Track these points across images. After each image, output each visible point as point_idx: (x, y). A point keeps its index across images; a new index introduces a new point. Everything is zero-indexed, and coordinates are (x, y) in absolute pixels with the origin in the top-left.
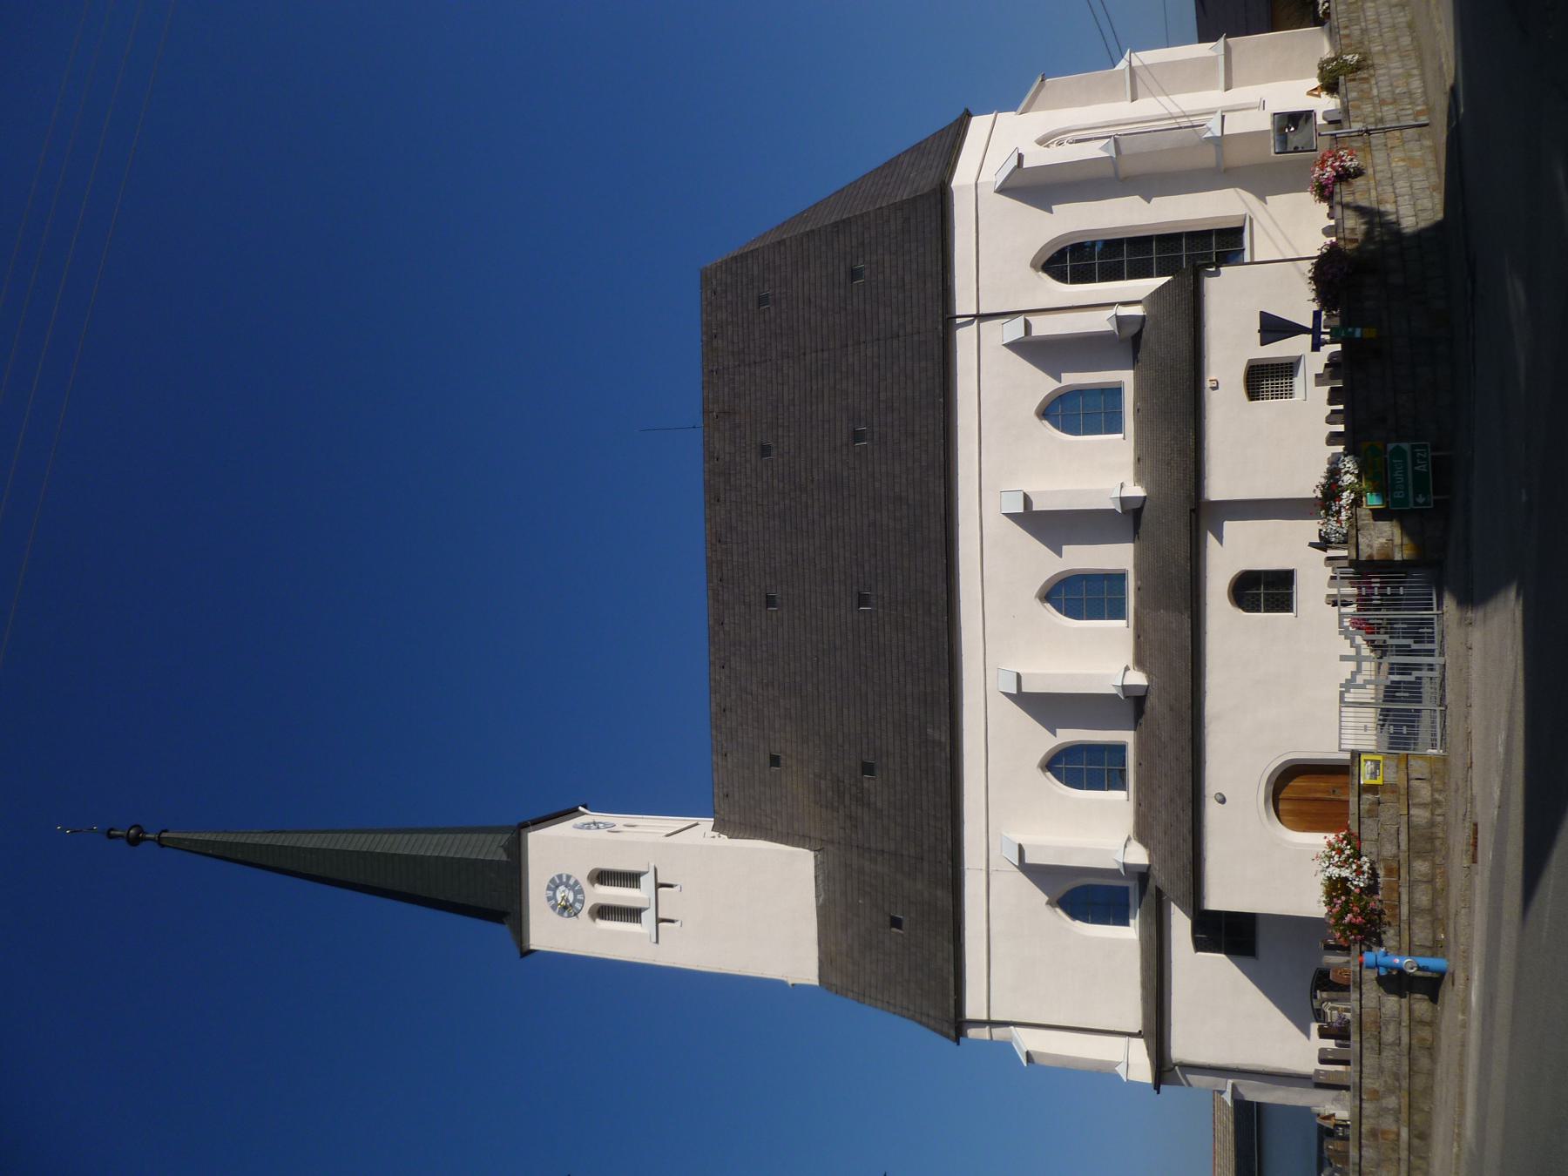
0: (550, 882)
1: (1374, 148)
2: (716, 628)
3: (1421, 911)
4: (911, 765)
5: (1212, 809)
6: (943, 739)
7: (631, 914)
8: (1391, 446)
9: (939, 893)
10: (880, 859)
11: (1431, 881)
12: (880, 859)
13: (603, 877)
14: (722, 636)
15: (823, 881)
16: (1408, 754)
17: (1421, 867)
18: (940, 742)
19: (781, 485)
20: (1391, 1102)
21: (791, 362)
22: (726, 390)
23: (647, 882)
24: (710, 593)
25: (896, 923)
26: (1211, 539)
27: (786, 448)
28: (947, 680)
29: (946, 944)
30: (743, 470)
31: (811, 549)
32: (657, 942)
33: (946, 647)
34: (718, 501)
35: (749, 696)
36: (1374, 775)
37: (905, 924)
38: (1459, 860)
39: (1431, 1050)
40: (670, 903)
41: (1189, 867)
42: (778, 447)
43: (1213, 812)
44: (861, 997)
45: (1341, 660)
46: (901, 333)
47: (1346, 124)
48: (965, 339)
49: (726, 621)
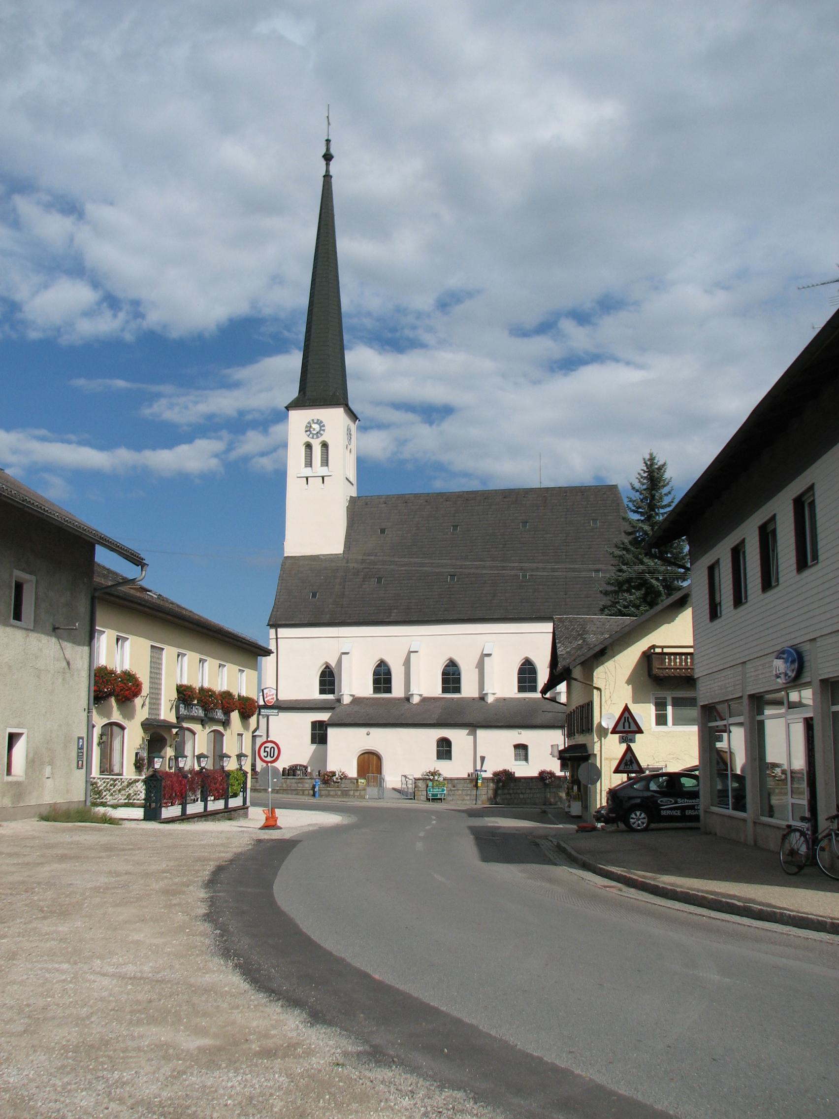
2: (444, 497)
3: (329, 792)
4: (381, 602)
5: (364, 731)
6: (392, 617)
7: (309, 463)
8: (445, 788)
9: (328, 616)
10: (341, 587)
11: (336, 795)
12: (341, 587)
13: (325, 445)
14: (441, 500)
15: (330, 558)
17: (339, 793)
18: (390, 616)
19: (507, 534)
20: (284, 785)
21: (564, 538)
22: (556, 501)
23: (323, 471)
24: (461, 493)
25: (314, 595)
26: (467, 731)
27: (524, 536)
28: (416, 619)
29: (308, 619)
30: (517, 512)
31: (477, 550)
32: (298, 477)
33: (430, 619)
34: (504, 498)
35: (412, 516)
36: (361, 782)
37: (314, 599)
38: (340, 800)
39: (297, 794)
40: (315, 482)
41: (343, 722)
42: (525, 531)
43: (363, 731)
44: (281, 578)
46: (567, 596)
49: (448, 502)
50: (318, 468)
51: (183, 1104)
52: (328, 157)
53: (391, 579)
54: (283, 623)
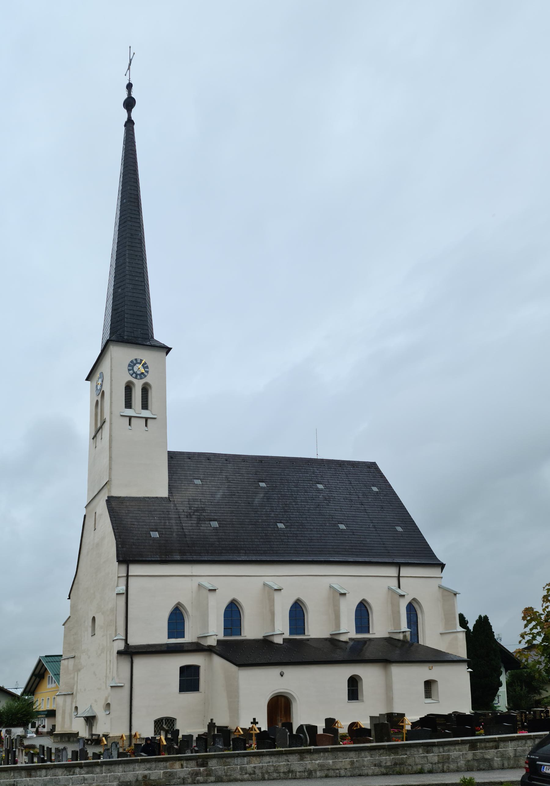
0: (147, 366)
1: (185, 516)
13: (145, 390)
16: (134, 771)
32: (122, 416)
40: (138, 424)
45: (253, 719)
47: (498, 704)
48: (392, 571)
50: (137, 409)
51: (537, 649)
52: (129, 104)
53: (143, 523)
54: (150, 559)
